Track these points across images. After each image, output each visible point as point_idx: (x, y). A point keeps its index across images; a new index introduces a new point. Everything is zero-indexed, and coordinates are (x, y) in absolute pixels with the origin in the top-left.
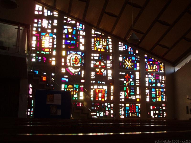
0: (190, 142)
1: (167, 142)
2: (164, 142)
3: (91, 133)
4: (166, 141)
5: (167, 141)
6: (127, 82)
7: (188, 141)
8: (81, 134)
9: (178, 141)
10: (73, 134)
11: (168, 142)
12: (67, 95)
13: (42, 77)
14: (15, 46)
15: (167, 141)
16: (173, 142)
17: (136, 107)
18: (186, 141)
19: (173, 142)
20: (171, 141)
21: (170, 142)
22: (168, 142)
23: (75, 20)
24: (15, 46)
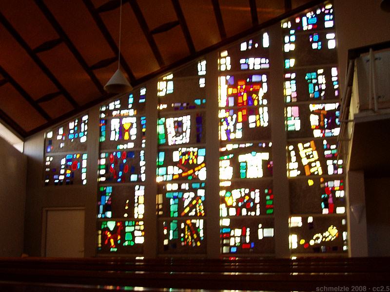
0: (388, 289)
1: (341, 289)
2: (336, 289)
3: (248, 275)
4: (340, 289)
5: (342, 288)
6: (139, 173)
7: (385, 288)
8: (294, 274)
9: (364, 288)
10: (86, 287)
11: (343, 289)
12: (108, 200)
13: (125, 161)
14: (376, 59)
15: (342, 288)
16: (355, 289)
17: (268, 214)
18: (381, 289)
19: (355, 289)
20: (351, 289)
21: (347, 289)
22: (343, 289)
23: (263, 30)
24: (376, 59)
